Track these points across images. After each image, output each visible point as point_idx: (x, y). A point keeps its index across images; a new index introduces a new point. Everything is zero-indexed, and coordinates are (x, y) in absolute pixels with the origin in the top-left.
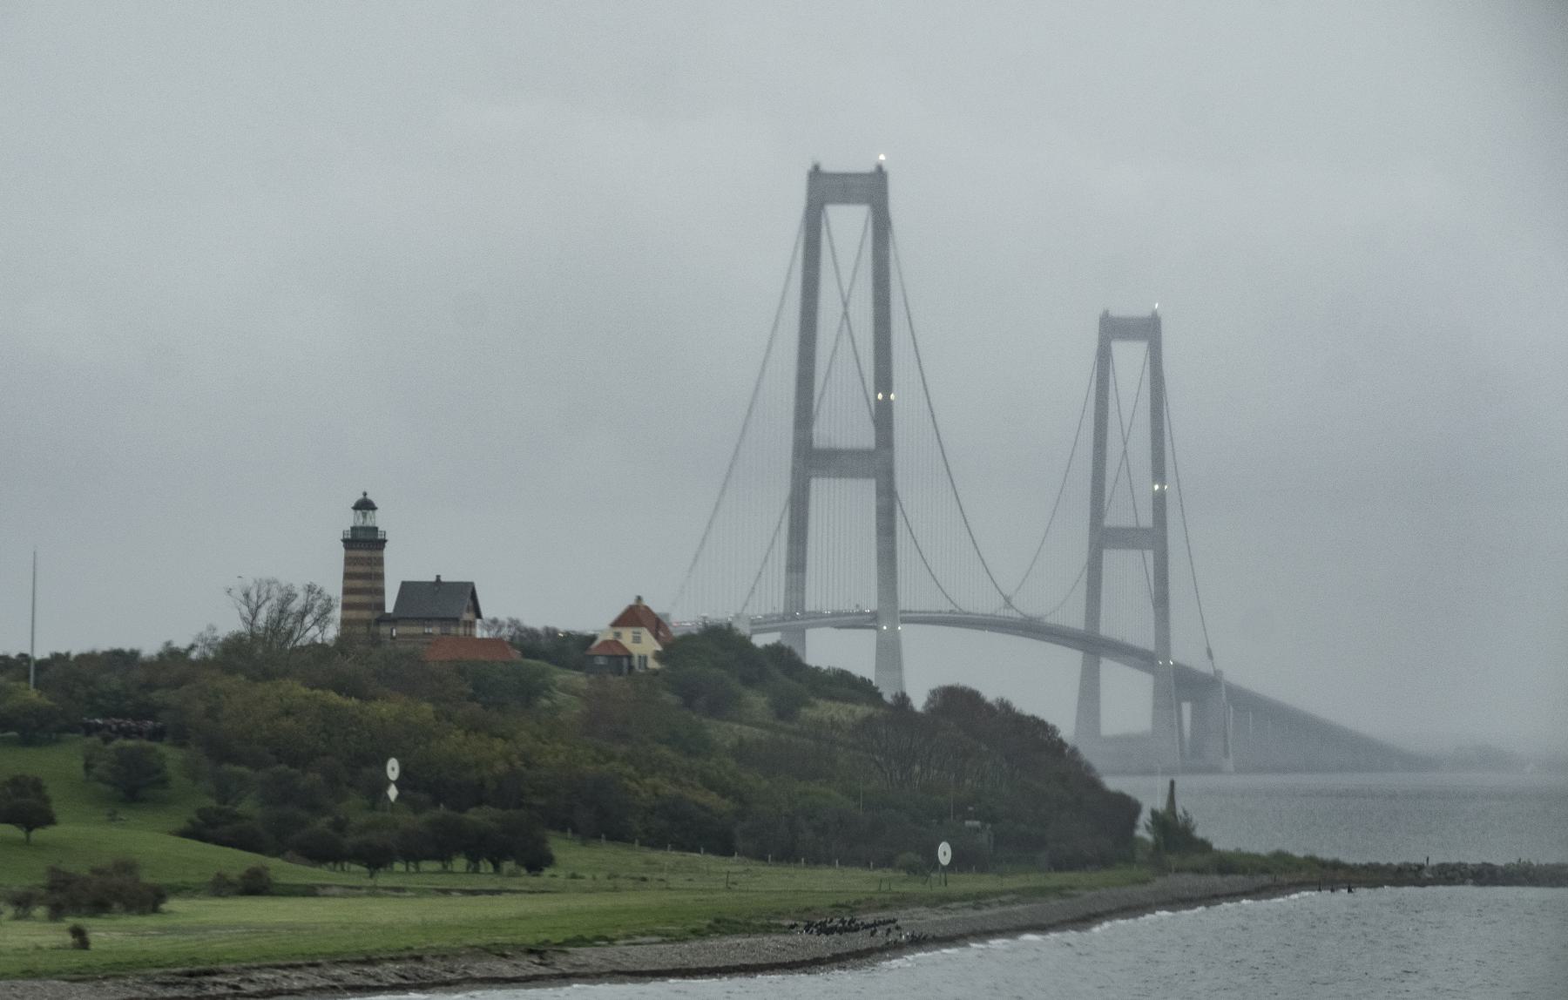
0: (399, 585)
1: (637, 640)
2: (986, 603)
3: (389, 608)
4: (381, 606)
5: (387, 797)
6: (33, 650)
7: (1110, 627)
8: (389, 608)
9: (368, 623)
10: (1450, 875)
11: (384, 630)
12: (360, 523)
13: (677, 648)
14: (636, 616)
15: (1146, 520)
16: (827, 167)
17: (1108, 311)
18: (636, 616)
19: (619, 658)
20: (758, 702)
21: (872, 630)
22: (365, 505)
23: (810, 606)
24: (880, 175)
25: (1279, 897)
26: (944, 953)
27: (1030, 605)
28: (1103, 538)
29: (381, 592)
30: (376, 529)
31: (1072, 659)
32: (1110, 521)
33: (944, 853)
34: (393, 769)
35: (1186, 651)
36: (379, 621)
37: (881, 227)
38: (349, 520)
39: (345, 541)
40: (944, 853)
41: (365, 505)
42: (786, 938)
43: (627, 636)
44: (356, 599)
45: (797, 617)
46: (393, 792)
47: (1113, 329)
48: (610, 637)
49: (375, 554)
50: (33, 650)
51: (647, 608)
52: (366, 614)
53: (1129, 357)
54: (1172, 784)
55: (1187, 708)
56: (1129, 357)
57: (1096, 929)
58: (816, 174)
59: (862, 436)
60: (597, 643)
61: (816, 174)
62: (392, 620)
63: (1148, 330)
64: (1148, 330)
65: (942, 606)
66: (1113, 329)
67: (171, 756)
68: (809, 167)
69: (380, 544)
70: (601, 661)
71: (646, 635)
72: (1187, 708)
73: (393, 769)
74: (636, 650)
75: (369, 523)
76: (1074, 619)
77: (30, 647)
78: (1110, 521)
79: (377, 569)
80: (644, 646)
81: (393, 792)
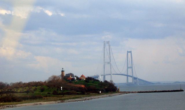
6: (133, 74)
7: (129, 75)
10: (161, 92)
14: (82, 76)
15: (131, 66)
21: (129, 75)
22: (63, 69)
27: (122, 73)
28: (128, 68)
31: (126, 77)
32: (128, 66)
33: (100, 92)
34: (62, 88)
35: (135, 76)
38: (62, 70)
40: (100, 92)
46: (62, 89)
47: (128, 52)
50: (133, 74)
53: (129, 54)
55: (135, 80)
56: (129, 54)
63: (131, 52)
64: (131, 52)
65: (116, 73)
66: (128, 52)
72: (135, 80)
73: (62, 88)
77: (132, 74)
78: (128, 66)
81: (62, 89)
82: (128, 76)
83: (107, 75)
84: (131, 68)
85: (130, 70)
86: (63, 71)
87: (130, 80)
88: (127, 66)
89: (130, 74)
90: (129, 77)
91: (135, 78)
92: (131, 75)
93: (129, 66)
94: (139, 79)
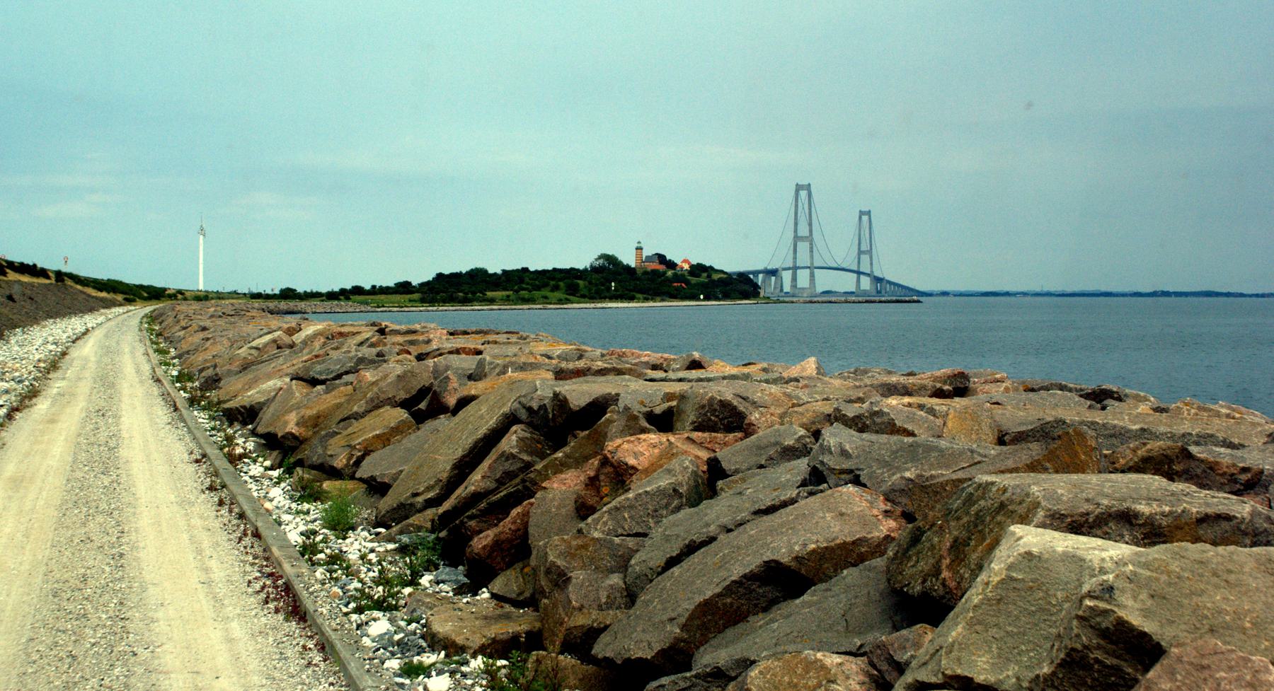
2: (835, 265)
27: (844, 266)
35: (878, 273)
38: (637, 245)
61: (860, 211)
63: (869, 213)
80: (686, 267)
82: (859, 273)
85: (865, 258)
86: (639, 249)
88: (859, 249)
89: (865, 268)
91: (878, 280)
92: (868, 271)
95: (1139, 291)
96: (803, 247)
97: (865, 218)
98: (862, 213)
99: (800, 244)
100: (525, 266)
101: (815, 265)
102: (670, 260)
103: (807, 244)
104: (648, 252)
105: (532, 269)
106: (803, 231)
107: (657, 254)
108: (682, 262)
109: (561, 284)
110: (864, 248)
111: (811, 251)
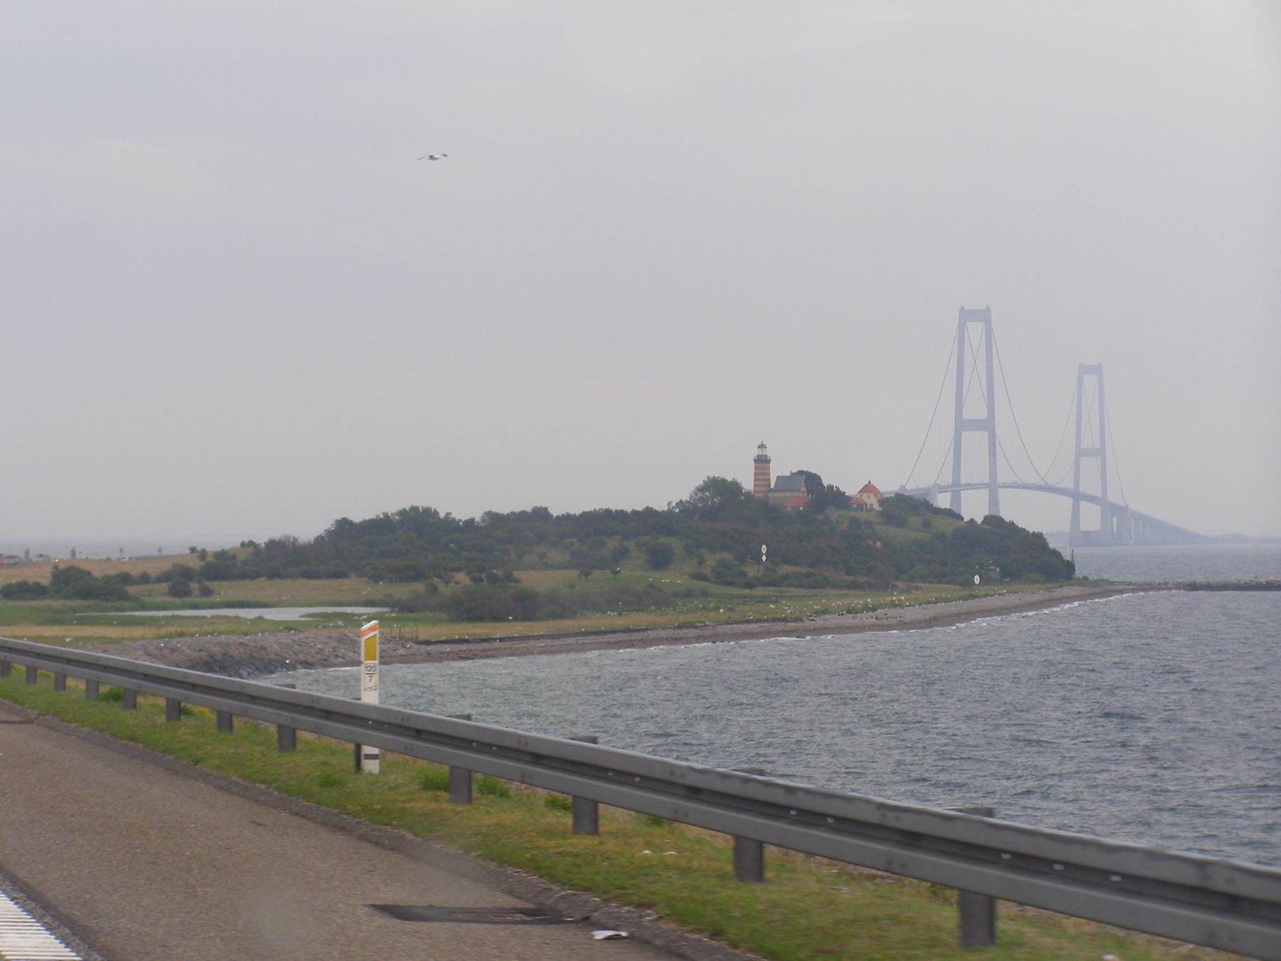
0: (776, 477)
1: (869, 497)
2: (1034, 480)
3: (772, 487)
4: (770, 486)
5: (762, 560)
7: (1085, 488)
8: (772, 487)
9: (764, 492)
11: (770, 495)
12: (760, 453)
13: (884, 502)
14: (868, 488)
15: (1098, 445)
16: (966, 308)
17: (1081, 363)
18: (868, 488)
19: (861, 506)
20: (915, 520)
21: (1089, 492)
22: (762, 446)
23: (962, 482)
24: (988, 310)
25: (744, 640)
26: (782, 644)
27: (1052, 481)
29: (769, 480)
30: (766, 456)
32: (1084, 445)
33: (977, 579)
34: (764, 549)
35: (1113, 497)
36: (768, 492)
37: (989, 331)
38: (756, 452)
39: (755, 461)
40: (977, 579)
41: (762, 446)
42: (777, 627)
43: (865, 497)
44: (758, 482)
45: (956, 488)
46: (764, 558)
48: (858, 497)
49: (767, 465)
51: (873, 486)
52: (764, 489)
54: (1073, 551)
55: (1115, 519)
56: (1090, 381)
57: (1162, 592)
58: (962, 310)
59: (982, 414)
60: (853, 500)
61: (962, 310)
62: (771, 490)
63: (1097, 370)
66: (966, 316)
67: (675, 543)
68: (960, 307)
69: (769, 461)
70: (855, 506)
71: (872, 496)
72: (1115, 519)
73: (764, 549)
74: (868, 502)
75: (764, 453)
76: (1069, 484)
78: (1084, 445)
79: (768, 471)
80: (872, 501)
81: (764, 558)
82: (1077, 496)
83: (1005, 486)
84: (1100, 452)
85: (975, 442)
86: (762, 462)
87: (1091, 518)
88: (1078, 444)
89: (1090, 485)
90: (1083, 504)
91: (1113, 510)
92: (1098, 493)
93: (1085, 444)
94: (1138, 517)
95: (1210, 581)
96: (975, 442)
97: (975, 330)
98: (1084, 370)
99: (1084, 460)
100: (541, 503)
101: (1000, 480)
102: (831, 487)
103: (983, 436)
104: (778, 470)
105: (556, 511)
106: (973, 408)
107: (801, 473)
108: (863, 491)
109: (631, 544)
110: (973, 408)
111: (993, 453)
